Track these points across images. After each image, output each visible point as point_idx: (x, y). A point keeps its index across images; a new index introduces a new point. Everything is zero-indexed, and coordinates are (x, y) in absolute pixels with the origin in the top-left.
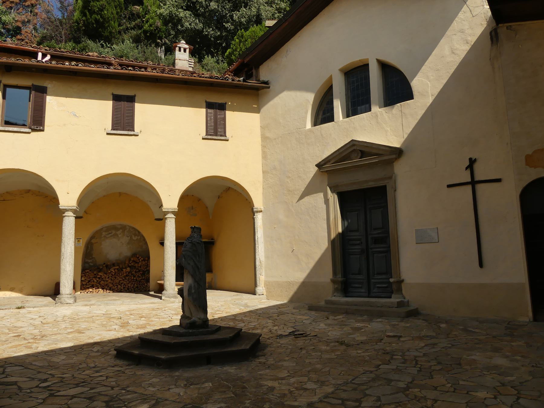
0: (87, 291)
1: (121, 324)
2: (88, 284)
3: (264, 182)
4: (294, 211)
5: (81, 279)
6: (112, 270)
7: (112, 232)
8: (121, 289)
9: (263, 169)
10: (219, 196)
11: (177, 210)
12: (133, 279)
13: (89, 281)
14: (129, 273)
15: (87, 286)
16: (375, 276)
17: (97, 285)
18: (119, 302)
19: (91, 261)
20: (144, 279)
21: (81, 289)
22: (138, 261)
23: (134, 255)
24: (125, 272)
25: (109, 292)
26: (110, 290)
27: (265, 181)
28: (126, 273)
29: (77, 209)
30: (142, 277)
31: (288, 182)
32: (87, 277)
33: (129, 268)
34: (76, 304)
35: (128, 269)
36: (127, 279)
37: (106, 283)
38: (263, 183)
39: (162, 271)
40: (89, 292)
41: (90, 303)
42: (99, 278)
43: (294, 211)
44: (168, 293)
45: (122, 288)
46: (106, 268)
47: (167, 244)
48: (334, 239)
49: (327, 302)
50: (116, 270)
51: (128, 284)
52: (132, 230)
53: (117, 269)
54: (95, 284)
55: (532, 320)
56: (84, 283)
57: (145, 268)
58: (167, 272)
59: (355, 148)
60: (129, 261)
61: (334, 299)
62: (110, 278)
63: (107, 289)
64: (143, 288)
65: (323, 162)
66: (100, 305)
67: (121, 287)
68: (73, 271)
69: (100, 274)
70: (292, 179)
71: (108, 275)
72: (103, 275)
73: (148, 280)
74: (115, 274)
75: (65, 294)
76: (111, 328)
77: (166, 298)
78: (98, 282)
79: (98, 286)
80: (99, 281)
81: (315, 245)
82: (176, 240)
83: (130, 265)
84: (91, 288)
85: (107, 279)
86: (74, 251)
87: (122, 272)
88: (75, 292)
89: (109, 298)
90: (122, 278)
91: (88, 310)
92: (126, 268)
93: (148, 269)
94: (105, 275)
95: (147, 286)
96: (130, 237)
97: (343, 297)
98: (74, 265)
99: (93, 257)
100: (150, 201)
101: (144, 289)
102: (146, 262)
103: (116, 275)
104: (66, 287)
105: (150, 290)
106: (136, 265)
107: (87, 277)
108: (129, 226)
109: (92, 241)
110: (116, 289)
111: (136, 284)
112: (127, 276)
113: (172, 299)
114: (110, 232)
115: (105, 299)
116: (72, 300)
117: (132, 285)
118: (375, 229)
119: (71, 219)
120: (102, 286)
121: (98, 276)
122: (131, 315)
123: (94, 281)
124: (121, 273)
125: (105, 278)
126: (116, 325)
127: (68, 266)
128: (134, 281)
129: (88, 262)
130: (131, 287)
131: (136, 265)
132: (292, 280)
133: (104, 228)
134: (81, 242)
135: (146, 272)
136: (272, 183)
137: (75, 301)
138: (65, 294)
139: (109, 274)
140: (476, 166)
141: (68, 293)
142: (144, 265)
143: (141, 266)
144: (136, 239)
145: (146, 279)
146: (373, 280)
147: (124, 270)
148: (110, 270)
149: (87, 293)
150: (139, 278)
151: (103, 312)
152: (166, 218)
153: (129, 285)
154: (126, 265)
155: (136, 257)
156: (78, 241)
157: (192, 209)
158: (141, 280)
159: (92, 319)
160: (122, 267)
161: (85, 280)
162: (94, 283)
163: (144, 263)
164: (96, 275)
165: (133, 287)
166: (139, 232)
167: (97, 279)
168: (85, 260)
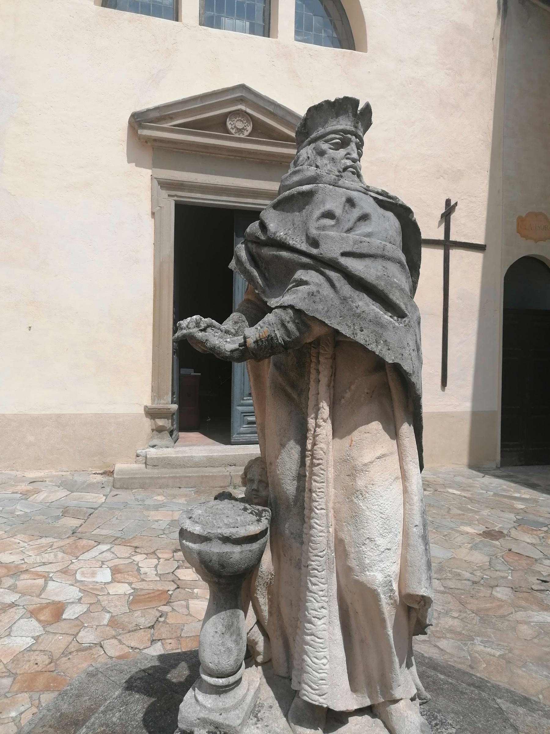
16: (245, 398)
55: (499, 466)
65: (157, 114)
140: (454, 217)
146: (240, 408)
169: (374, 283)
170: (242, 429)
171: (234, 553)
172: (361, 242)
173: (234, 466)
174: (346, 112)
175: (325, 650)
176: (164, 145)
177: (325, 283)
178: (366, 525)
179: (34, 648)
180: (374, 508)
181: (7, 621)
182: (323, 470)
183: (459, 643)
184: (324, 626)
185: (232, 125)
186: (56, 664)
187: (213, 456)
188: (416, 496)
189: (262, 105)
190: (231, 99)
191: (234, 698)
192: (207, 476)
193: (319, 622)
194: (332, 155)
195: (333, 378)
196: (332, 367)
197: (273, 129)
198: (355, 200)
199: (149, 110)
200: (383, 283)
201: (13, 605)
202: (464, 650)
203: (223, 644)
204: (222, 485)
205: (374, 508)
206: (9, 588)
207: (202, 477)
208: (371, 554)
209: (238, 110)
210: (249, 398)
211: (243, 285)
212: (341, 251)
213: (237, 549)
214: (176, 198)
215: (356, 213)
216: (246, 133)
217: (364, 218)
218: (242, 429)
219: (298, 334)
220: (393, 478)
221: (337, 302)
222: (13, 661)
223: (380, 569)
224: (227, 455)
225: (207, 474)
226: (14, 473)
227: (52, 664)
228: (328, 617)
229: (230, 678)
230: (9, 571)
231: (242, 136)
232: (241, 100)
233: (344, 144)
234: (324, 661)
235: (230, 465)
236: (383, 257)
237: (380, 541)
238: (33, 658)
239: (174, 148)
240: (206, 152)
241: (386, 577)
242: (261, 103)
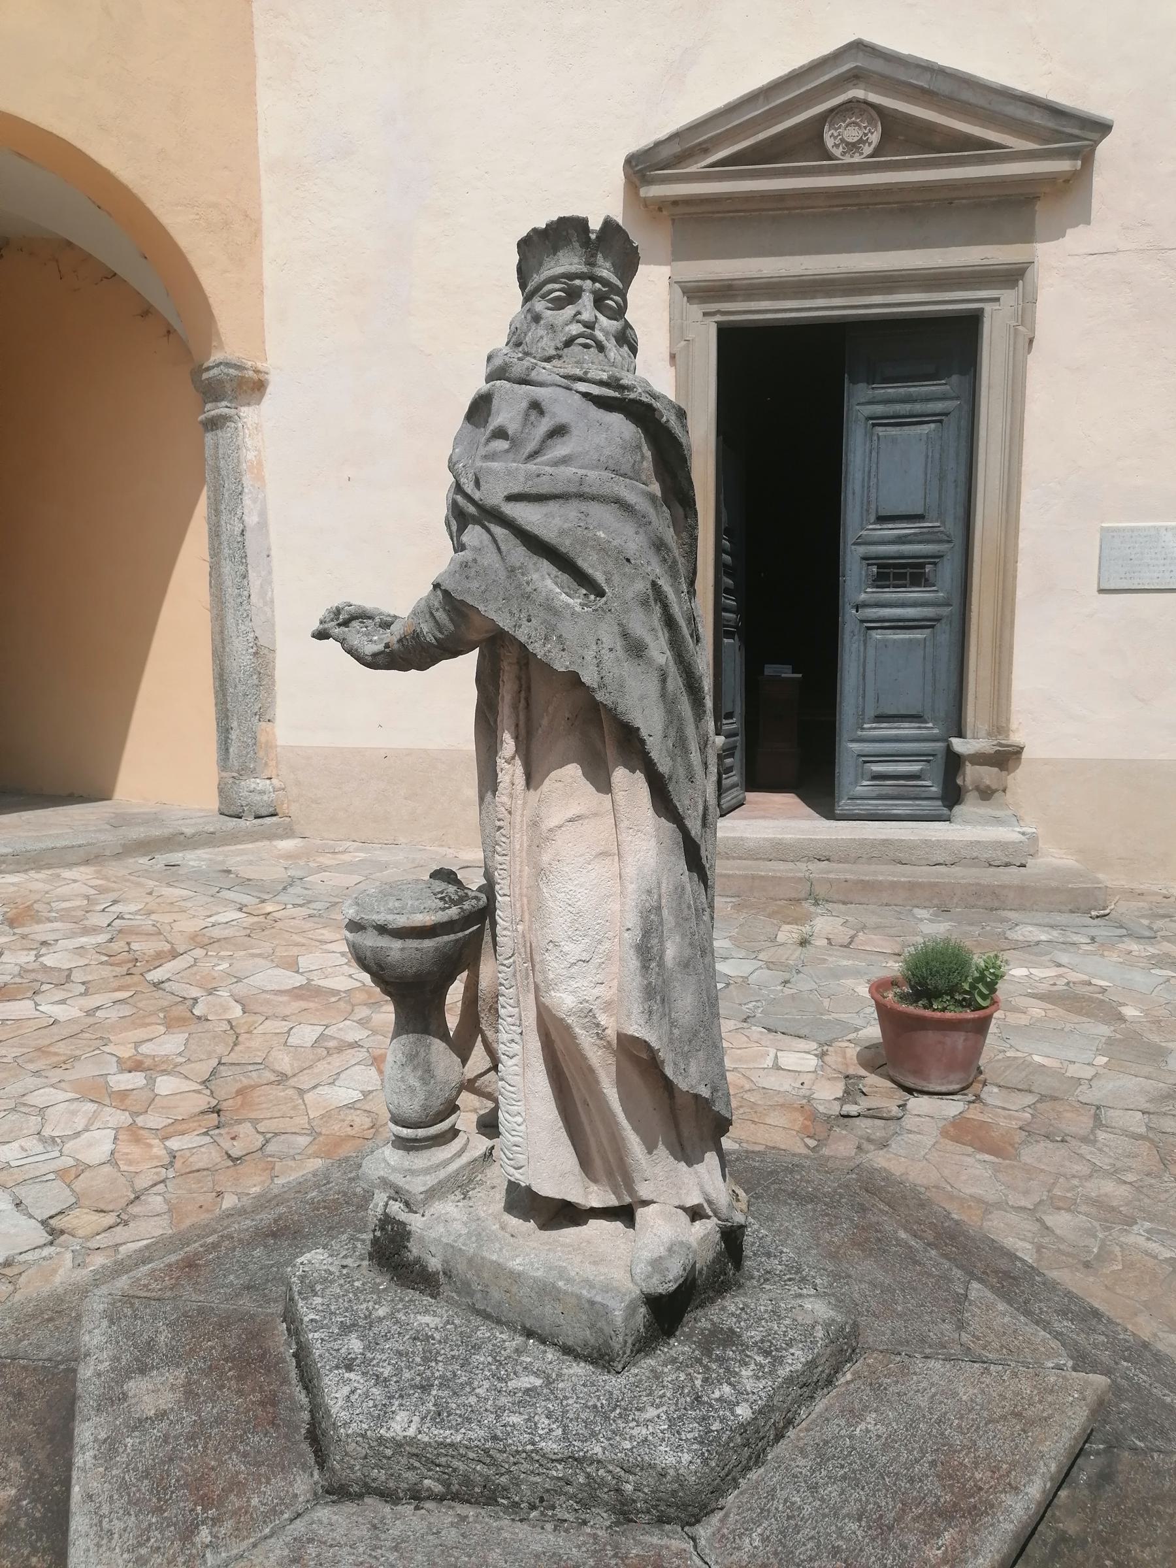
16: (866, 726)
59: (859, 93)
65: (676, 149)
118: (882, 519)
146: (855, 746)
169: (554, 542)
170: (859, 789)
171: (391, 949)
172: (538, 476)
173: (826, 862)
174: (568, 242)
175: (519, 1104)
176: (692, 210)
177: (490, 545)
178: (549, 921)
179: (358, 1105)
180: (561, 896)
181: (338, 1064)
182: (504, 836)
183: (1096, 1224)
184: (516, 1068)
185: (835, 138)
186: (377, 1130)
187: (782, 839)
188: (632, 883)
189: (903, 78)
190: (831, 79)
191: (429, 1160)
192: (762, 877)
193: (510, 1062)
194: (551, 319)
195: (523, 694)
196: (519, 678)
197: (931, 128)
198: (543, 403)
199: (658, 144)
200: (567, 542)
201: (355, 1045)
202: (1095, 1237)
203: (403, 1079)
204: (793, 895)
205: (561, 896)
206: (359, 1022)
207: (753, 877)
208: (555, 965)
209: (850, 101)
210: (874, 725)
211: (863, 487)
212: (505, 494)
213: (397, 944)
214: (719, 318)
215: (545, 425)
216: (868, 150)
217: (559, 431)
218: (858, 788)
219: (452, 628)
220: (594, 853)
221: (503, 574)
222: (323, 1116)
223: (570, 989)
224: (811, 839)
225: (763, 873)
226: (442, 850)
227: (373, 1131)
228: (521, 1056)
229: (419, 1130)
230: (370, 998)
231: (857, 159)
232: (855, 77)
233: (573, 296)
234: (519, 1119)
235: (819, 860)
236: (581, 496)
237: (568, 947)
238: (350, 1118)
239: (713, 213)
240: (780, 209)
241: (581, 1003)
242: (901, 75)
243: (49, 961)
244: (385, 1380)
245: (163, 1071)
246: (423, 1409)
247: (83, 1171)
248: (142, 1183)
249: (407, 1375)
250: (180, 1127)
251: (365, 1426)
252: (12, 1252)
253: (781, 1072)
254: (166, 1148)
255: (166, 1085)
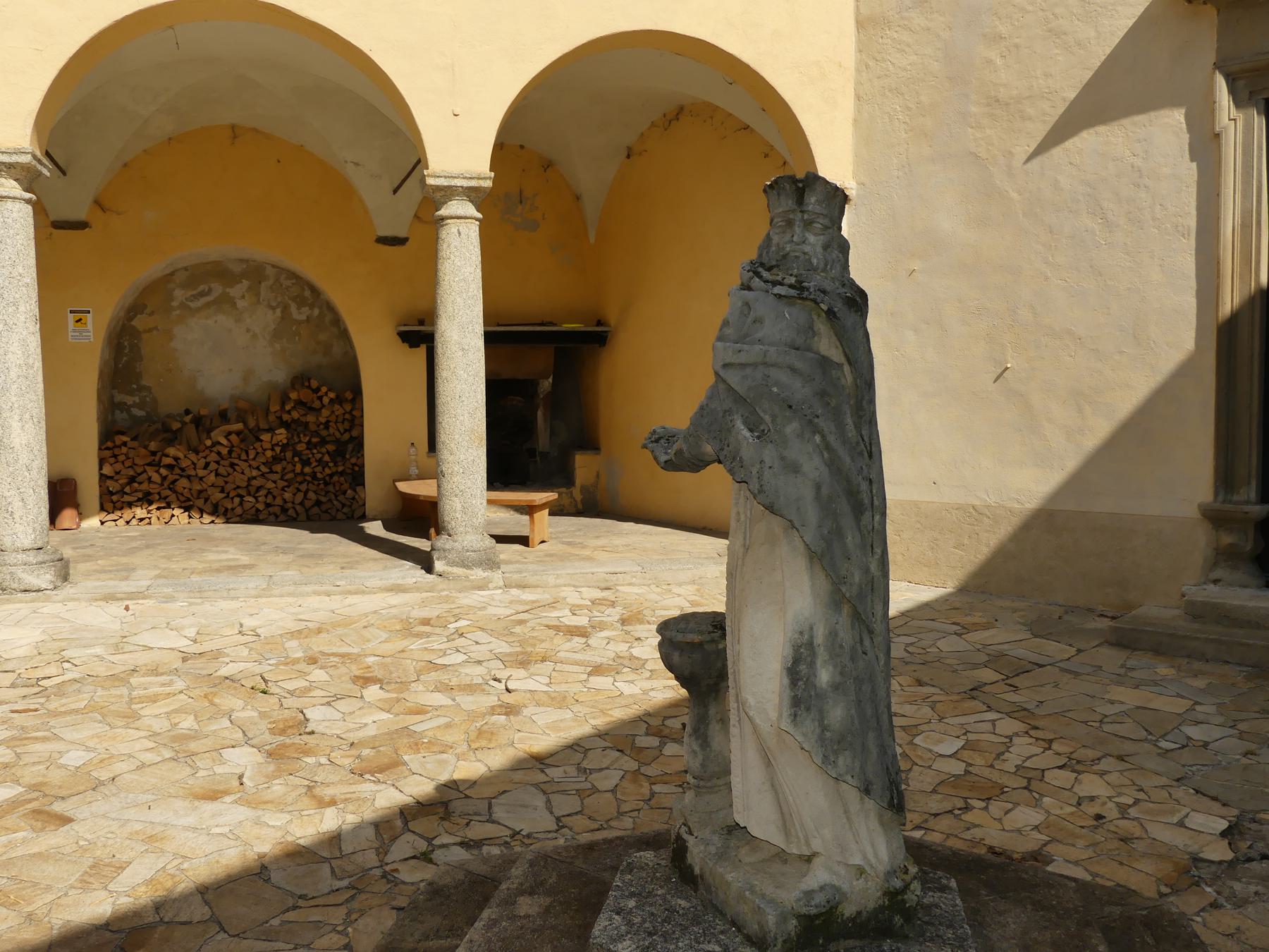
0: (127, 514)
1: (267, 737)
2: (127, 489)
3: (862, 67)
4: (1015, 195)
5: (101, 468)
6: (218, 435)
7: (210, 290)
8: (258, 510)
9: (857, 8)
10: (629, 149)
11: (488, 184)
12: (302, 473)
13: (132, 480)
14: (284, 448)
15: (127, 498)
17: (163, 496)
18: (252, 582)
19: (137, 399)
20: (342, 474)
21: (102, 509)
22: (317, 404)
23: (300, 380)
24: (269, 446)
25: (213, 522)
26: (215, 512)
27: (871, 63)
28: (273, 449)
29: (39, 167)
30: (336, 464)
31: (989, 62)
32: (123, 462)
33: (282, 431)
34: (68, 590)
35: (282, 435)
36: (277, 473)
37: (199, 487)
38: (858, 71)
39: (413, 444)
40: (134, 522)
41: (125, 587)
42: (170, 467)
43: (1015, 195)
44: (460, 547)
45: (261, 507)
46: (197, 428)
47: (448, 334)
48: (1234, 318)
49: (1197, 612)
50: (233, 437)
51: (283, 489)
52: (289, 283)
53: (238, 433)
54: (154, 488)
56: (113, 486)
57: (346, 431)
58: (451, 458)
60: (283, 404)
61: (1213, 593)
62: (213, 466)
63: (202, 512)
64: (339, 506)
66: (169, 599)
67: (257, 501)
68: (44, 449)
69: (172, 451)
70: (1017, 46)
71: (205, 458)
72: (185, 457)
73: (358, 478)
74: (230, 452)
75: (16, 551)
76: (219, 770)
77: (449, 569)
78: (166, 484)
79: (167, 497)
80: (171, 478)
81: (1121, 352)
82: (486, 323)
83: (286, 417)
84: (139, 503)
85: (201, 473)
86: (40, 357)
87: (257, 445)
88: (81, 520)
89: (211, 557)
90: (258, 468)
91: (117, 626)
92: (271, 430)
93: (355, 433)
94: (193, 457)
95: (354, 498)
96: (282, 312)
97: (1259, 587)
98: (43, 423)
99: (144, 382)
100: (357, 164)
101: (345, 510)
102: (348, 407)
103: (234, 455)
104: (17, 519)
105: (367, 513)
106: (311, 418)
107: (123, 462)
108: (273, 266)
109: (133, 323)
110: (239, 511)
111: (315, 492)
112: (276, 460)
113: (478, 574)
114: (201, 288)
115: (193, 564)
116: (48, 577)
117: (300, 497)
119: (15, 215)
120: (182, 499)
121: (164, 458)
122: (313, 661)
123: (150, 478)
124: (254, 448)
125: (195, 469)
126: (248, 741)
127: (16, 425)
128: (305, 480)
129: (125, 403)
130: (293, 503)
131: (311, 418)
132: (991, 500)
133: (177, 270)
134: (90, 326)
135: (350, 447)
136: (905, 70)
137: (65, 577)
138: (16, 551)
139: (207, 452)
141: (27, 542)
142: (340, 419)
143: (328, 422)
144: (304, 318)
145: (349, 471)
147: (266, 437)
148: (210, 438)
149: (128, 523)
150: (323, 468)
151: (182, 643)
152: (443, 219)
153: (287, 496)
154: (272, 418)
155: (309, 387)
156: (77, 321)
157: (521, 202)
158: (331, 476)
159: (124, 691)
160: (257, 425)
161: (118, 473)
162: (151, 485)
163: (338, 410)
164: (159, 455)
165: (301, 504)
166: (315, 291)
167: (163, 471)
168: (113, 397)
243: (635, 652)
244: (634, 924)
245: (673, 739)
246: (641, 943)
247: (594, 793)
248: (625, 808)
249: (647, 925)
250: (665, 778)
251: (604, 941)
252: (532, 831)
253: (1184, 830)
254: (651, 789)
255: (671, 749)
